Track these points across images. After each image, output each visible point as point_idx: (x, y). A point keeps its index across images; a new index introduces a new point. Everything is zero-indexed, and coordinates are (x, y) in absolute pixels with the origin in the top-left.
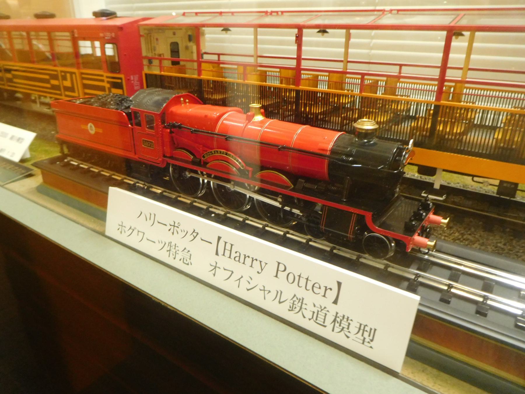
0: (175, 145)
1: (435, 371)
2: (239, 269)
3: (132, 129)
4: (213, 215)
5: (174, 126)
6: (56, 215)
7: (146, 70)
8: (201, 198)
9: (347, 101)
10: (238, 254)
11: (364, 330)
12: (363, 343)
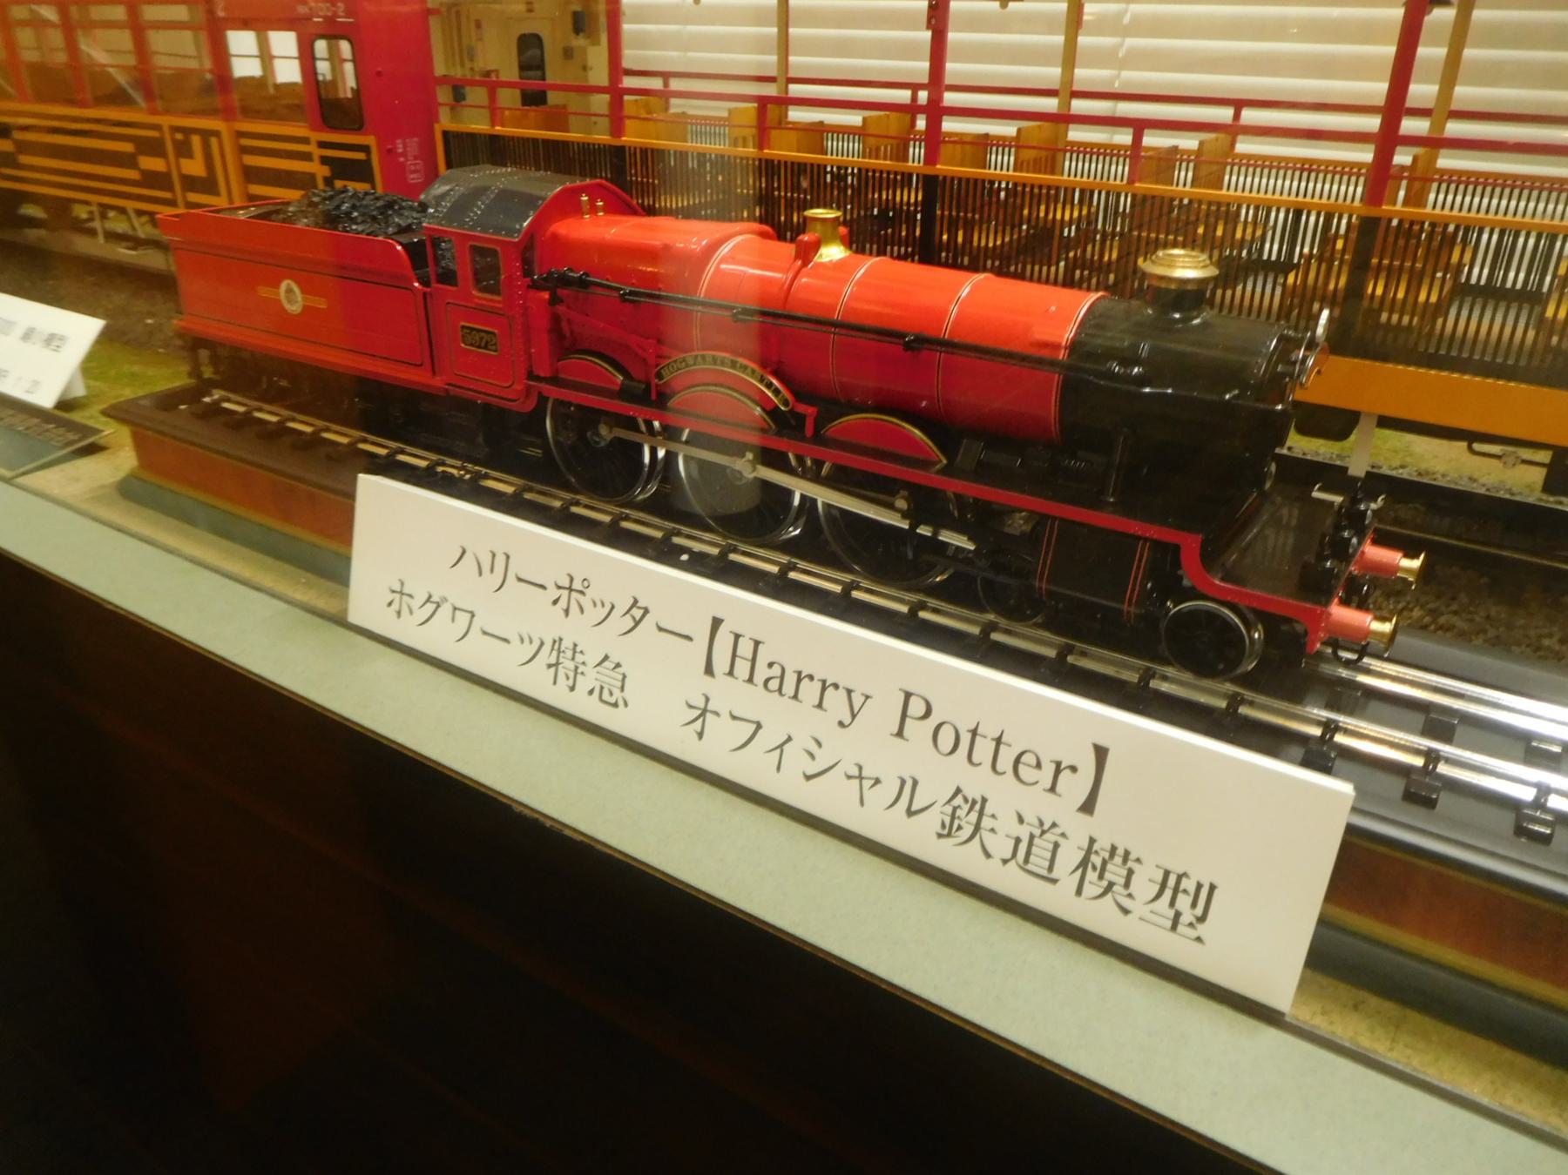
0: (565, 344)
1: (1389, 1007)
2: (780, 716)
3: (425, 295)
4: (685, 557)
5: (564, 281)
6: (187, 565)
7: (445, 121)
8: (646, 507)
9: (1067, 217)
10: (776, 671)
11: (1176, 891)
12: (1174, 927)
